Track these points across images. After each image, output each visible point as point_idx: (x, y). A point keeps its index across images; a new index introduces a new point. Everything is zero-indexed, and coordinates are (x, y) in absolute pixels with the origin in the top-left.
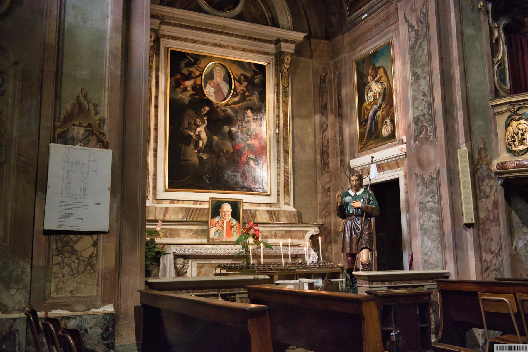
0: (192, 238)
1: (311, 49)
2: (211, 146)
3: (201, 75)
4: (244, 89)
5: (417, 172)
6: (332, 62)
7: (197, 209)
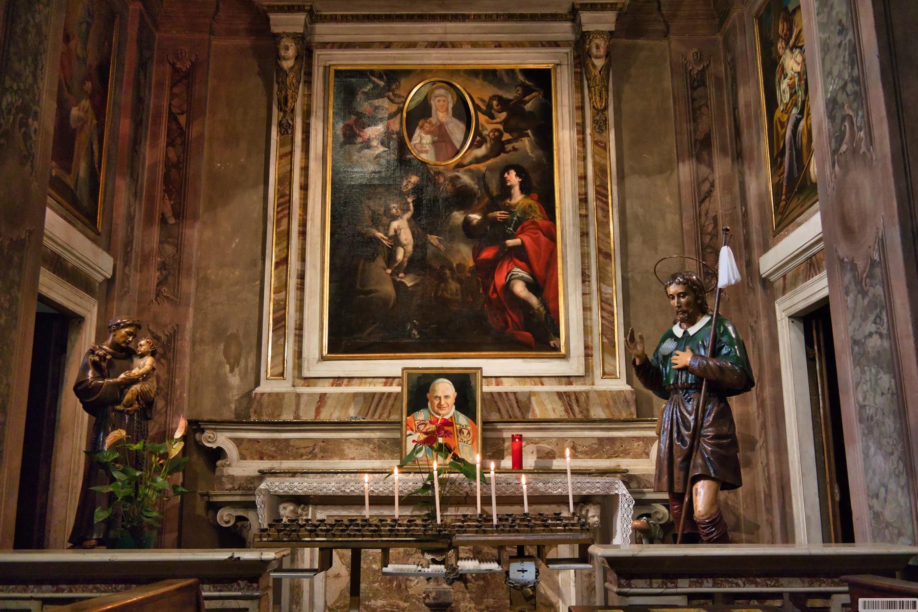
0: (371, 458)
1: (662, 15)
2: (423, 258)
3: (400, 110)
4: (501, 127)
5: (841, 253)
6: (720, 38)
7: (390, 394)
